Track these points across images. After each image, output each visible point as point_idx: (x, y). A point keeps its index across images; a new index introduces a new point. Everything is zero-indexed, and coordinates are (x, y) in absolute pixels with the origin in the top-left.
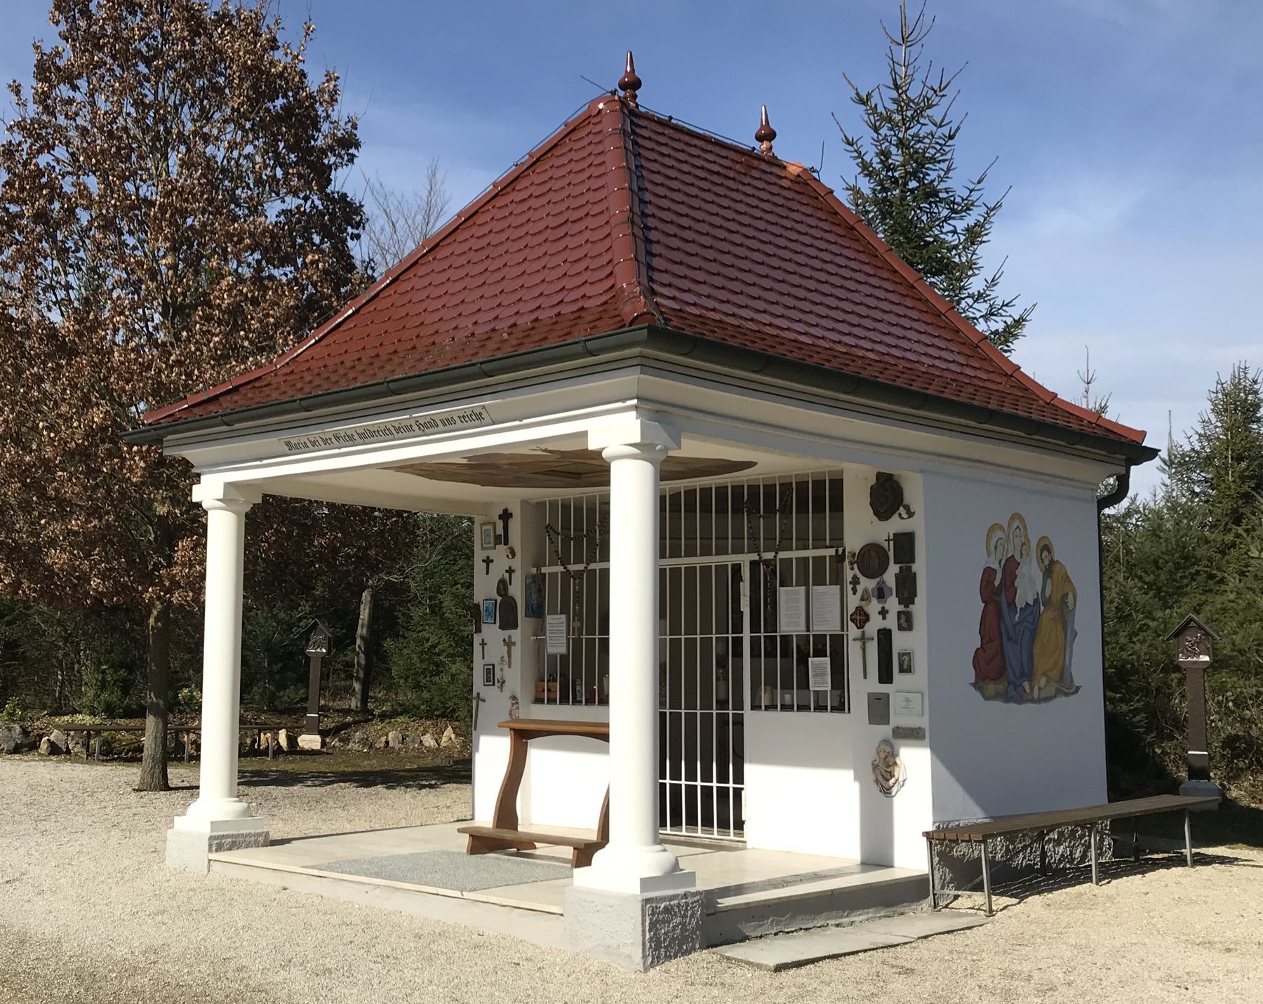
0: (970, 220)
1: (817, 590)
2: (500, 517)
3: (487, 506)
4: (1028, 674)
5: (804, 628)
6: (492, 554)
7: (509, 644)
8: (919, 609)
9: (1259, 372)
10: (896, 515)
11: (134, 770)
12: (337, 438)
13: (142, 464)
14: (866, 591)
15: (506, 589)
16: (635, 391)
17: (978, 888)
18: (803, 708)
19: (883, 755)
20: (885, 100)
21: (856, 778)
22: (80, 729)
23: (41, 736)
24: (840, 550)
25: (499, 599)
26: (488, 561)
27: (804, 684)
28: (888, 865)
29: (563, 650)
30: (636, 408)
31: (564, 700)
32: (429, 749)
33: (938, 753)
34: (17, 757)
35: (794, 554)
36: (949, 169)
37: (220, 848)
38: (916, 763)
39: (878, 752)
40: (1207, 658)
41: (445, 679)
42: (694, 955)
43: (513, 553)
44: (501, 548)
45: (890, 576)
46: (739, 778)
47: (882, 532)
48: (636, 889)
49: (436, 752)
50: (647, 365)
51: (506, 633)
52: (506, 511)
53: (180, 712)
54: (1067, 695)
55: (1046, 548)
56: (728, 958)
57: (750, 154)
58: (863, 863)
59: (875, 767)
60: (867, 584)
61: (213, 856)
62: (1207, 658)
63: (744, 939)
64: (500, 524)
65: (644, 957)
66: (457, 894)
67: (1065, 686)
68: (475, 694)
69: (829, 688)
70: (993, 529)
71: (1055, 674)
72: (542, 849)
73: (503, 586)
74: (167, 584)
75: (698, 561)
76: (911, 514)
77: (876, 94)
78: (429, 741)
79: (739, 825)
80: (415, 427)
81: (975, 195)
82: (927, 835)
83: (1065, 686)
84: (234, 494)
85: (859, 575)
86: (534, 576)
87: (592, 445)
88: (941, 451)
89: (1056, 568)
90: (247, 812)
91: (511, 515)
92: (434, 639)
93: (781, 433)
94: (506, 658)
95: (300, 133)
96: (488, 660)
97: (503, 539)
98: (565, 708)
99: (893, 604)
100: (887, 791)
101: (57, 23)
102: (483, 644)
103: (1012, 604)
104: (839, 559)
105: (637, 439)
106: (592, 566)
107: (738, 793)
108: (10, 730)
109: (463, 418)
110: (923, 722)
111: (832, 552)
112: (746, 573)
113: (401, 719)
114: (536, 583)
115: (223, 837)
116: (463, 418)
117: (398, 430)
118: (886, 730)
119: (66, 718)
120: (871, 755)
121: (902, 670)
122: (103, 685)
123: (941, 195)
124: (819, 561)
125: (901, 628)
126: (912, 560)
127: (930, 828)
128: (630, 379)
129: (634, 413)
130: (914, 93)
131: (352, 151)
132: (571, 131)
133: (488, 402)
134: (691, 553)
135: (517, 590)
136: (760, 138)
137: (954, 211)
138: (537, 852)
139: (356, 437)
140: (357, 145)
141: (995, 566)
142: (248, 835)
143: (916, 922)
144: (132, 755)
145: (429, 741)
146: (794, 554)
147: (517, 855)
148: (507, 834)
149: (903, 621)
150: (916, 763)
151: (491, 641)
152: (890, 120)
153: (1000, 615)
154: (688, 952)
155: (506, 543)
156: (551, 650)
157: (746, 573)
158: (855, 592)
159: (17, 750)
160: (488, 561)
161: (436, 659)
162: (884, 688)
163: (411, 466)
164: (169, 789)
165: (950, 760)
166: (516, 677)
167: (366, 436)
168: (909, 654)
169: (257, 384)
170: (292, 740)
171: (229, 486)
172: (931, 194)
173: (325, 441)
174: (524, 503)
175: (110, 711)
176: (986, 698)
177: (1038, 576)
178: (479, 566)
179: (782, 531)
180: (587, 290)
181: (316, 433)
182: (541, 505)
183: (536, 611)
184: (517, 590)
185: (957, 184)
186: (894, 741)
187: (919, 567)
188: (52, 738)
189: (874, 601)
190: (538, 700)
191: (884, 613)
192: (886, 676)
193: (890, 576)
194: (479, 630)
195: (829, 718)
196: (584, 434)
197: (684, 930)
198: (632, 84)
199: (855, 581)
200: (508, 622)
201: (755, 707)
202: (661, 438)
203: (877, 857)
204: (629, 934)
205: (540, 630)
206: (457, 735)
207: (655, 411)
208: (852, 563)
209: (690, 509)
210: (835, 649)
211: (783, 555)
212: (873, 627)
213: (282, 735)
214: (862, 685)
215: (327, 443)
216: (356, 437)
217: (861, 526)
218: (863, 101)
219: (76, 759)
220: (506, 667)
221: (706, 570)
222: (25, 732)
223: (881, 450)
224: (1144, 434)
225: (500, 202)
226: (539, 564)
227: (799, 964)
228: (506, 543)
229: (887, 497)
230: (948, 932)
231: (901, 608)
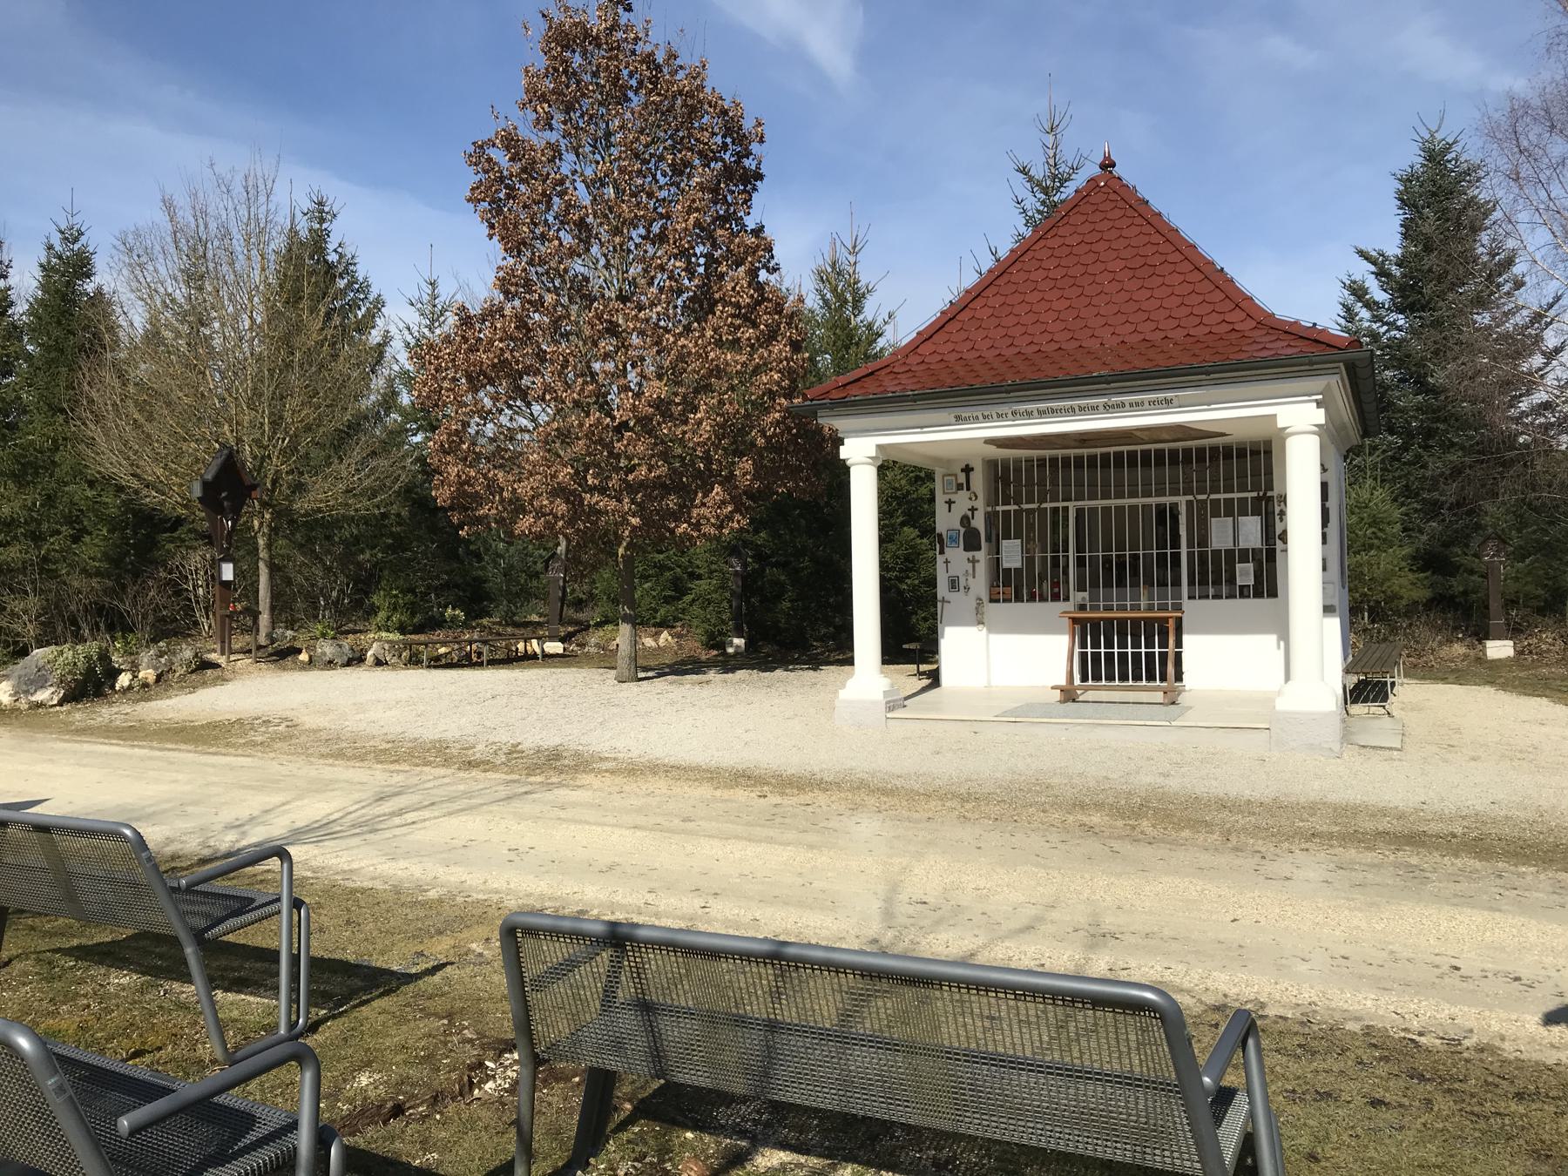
6: (953, 497)
7: (973, 561)
18: (1231, 596)
20: (1039, 172)
26: (950, 503)
29: (1018, 565)
44: (964, 494)
46: (1179, 644)
51: (970, 554)
64: (962, 478)
68: (939, 597)
73: (965, 521)
79: (1179, 676)
87: (1280, 424)
102: (947, 562)
107: (1178, 656)
109: (1152, 403)
111: (1255, 494)
112: (1183, 509)
114: (991, 518)
116: (1152, 403)
135: (979, 523)
140: (760, 177)
151: (953, 562)
156: (1006, 565)
157: (1183, 509)
159: (348, 664)
160: (950, 503)
166: (980, 584)
167: (1041, 413)
171: (880, 447)
175: (402, 629)
184: (979, 523)
194: (942, 552)
195: (1252, 603)
200: (972, 543)
201: (1191, 597)
211: (1213, 496)
219: (394, 667)
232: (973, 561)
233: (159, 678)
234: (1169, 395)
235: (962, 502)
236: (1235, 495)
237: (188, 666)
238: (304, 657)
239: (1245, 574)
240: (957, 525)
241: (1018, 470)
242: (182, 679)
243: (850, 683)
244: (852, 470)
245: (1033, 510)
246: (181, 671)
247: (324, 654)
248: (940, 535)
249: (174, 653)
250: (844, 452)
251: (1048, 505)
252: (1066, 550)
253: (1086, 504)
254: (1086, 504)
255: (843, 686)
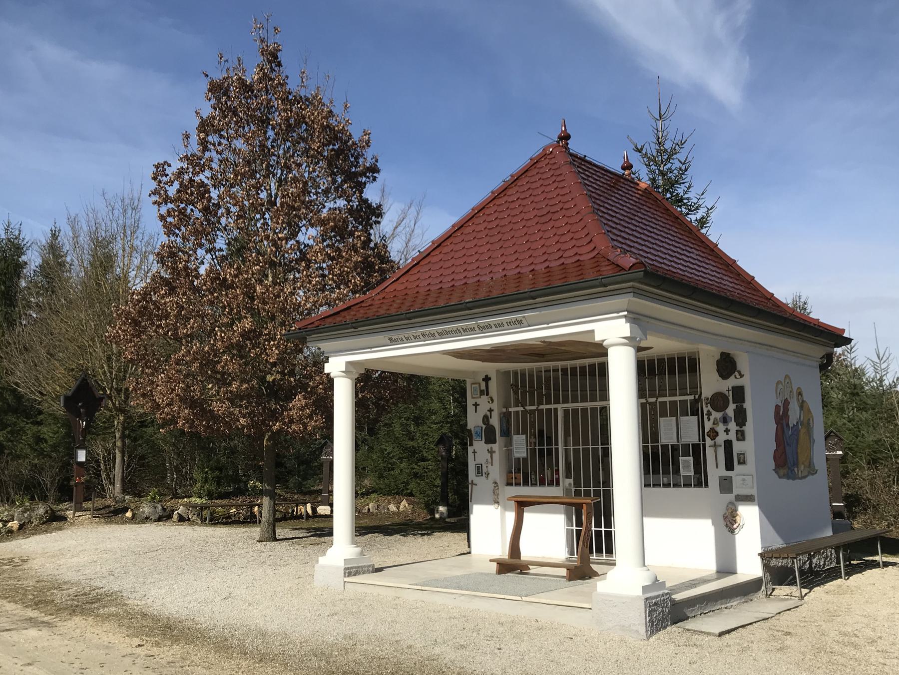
0: (699, 216)
1: (683, 419)
2: (483, 380)
3: (474, 373)
4: (796, 464)
5: (675, 440)
6: (478, 401)
7: (491, 452)
8: (749, 428)
9: (807, 298)
10: (733, 376)
11: (253, 529)
12: (423, 335)
13: (277, 352)
14: (716, 419)
15: (488, 421)
16: (626, 307)
17: (792, 583)
19: (730, 511)
20: (652, 149)
21: (713, 524)
22: (195, 506)
23: (173, 511)
24: (697, 397)
25: (484, 427)
26: (476, 405)
27: (677, 471)
28: (733, 572)
29: (525, 455)
30: (625, 316)
31: (526, 483)
32: (394, 513)
33: (764, 510)
34: (160, 523)
35: (668, 399)
36: (689, 187)
37: (350, 575)
38: (750, 516)
39: (727, 510)
40: (841, 453)
41: (397, 472)
42: (669, 628)
43: (493, 401)
44: (484, 397)
45: (730, 410)
47: (726, 386)
48: (639, 592)
49: (398, 513)
50: (638, 293)
51: (489, 446)
52: (486, 376)
53: (249, 495)
54: (813, 474)
55: (800, 394)
56: (688, 630)
57: (621, 177)
58: (718, 572)
59: (725, 518)
60: (716, 415)
61: (347, 579)
62: (841, 453)
63: (687, 618)
64: (483, 385)
65: (647, 631)
66: (519, 598)
67: (812, 471)
68: (470, 481)
69: (692, 474)
70: (778, 383)
71: (807, 464)
72: (533, 570)
73: (486, 419)
74: (287, 420)
75: (579, 405)
76: (742, 376)
77: (647, 146)
78: (392, 507)
79: (610, 551)
80: (477, 329)
81: (701, 202)
82: (761, 555)
83: (812, 471)
84: (352, 369)
85: (711, 410)
86: (504, 413)
87: (598, 338)
88: (760, 341)
89: (805, 404)
90: (362, 554)
91: (490, 379)
92: (389, 449)
93: (688, 330)
94: (490, 460)
95: (349, 164)
96: (478, 461)
97: (486, 392)
98: (526, 488)
99: (733, 426)
100: (732, 531)
101: (209, 100)
102: (474, 452)
103: (788, 425)
104: (696, 402)
105: (628, 335)
106: (541, 407)
107: (609, 535)
108: (155, 507)
109: (509, 323)
110: (754, 492)
111: (692, 397)
113: (373, 496)
114: (505, 417)
115: (351, 568)
116: (509, 323)
117: (465, 330)
118: (731, 497)
119: (186, 500)
120: (722, 510)
121: (739, 463)
122: (206, 481)
123: (685, 201)
124: (683, 402)
125: (738, 439)
126: (743, 401)
127: (760, 551)
128: (624, 300)
129: (624, 320)
130: (668, 145)
131: (375, 175)
132: (535, 163)
133: (528, 314)
134: (584, 400)
135: (495, 421)
136: (624, 168)
137: (690, 210)
138: (531, 571)
139: (436, 334)
140: (378, 171)
141: (780, 404)
142: (364, 566)
143: (760, 606)
144: (251, 520)
145: (392, 507)
146: (668, 399)
147: (521, 573)
148: (514, 561)
149: (739, 435)
150: (750, 516)
151: (479, 452)
152: (655, 161)
153: (783, 432)
154: (665, 627)
155: (487, 394)
156: (517, 455)
158: (709, 420)
159: (159, 519)
160: (476, 405)
161: (391, 461)
162: (729, 473)
163: (457, 353)
164: (277, 540)
165: (769, 514)
166: (496, 471)
167: (442, 334)
168: (743, 454)
169: (363, 305)
170: (314, 510)
171: (348, 364)
172: (679, 201)
173: (415, 337)
174: (498, 371)
175: (210, 496)
176: (780, 477)
177: (798, 409)
178: (470, 409)
179: (660, 386)
180: (580, 251)
181: (412, 332)
182: (507, 373)
183: (506, 433)
184: (495, 421)
185: (693, 195)
186: (736, 503)
187: (748, 405)
188: (179, 511)
189: (721, 425)
190: (509, 484)
191: (727, 431)
192: (729, 466)
193: (730, 410)
194: (471, 445)
196: (593, 331)
197: (663, 615)
198: (565, 137)
199: (709, 414)
200: (490, 439)
202: (639, 335)
203: (726, 568)
204: (638, 618)
205: (509, 444)
206: (409, 504)
207: (634, 318)
208: (707, 404)
209: (592, 374)
210: (697, 452)
211: (661, 399)
212: (722, 438)
213: (309, 506)
214: (715, 471)
215: (416, 338)
216: (436, 334)
217: (711, 383)
218: (640, 151)
220: (490, 465)
221: (584, 410)
222: (164, 509)
223: (731, 340)
224: (843, 330)
225: (497, 202)
226: (507, 405)
227: (729, 632)
228: (487, 394)
229: (727, 366)
230: (789, 610)
231: (738, 428)
232: (491, 452)
233: (21, 527)
234: (519, 316)
235: (483, 401)
236: (678, 398)
237: (41, 519)
238: (129, 514)
239: (687, 465)
240: (481, 424)
241: (539, 378)
242: (35, 529)
243: (330, 552)
244: (336, 380)
245: (534, 411)
246: (36, 522)
247: (143, 512)
248: (470, 431)
249: (33, 511)
250: (328, 368)
251: (544, 407)
252: (557, 444)
253: (571, 406)
254: (571, 406)
255: (324, 554)
